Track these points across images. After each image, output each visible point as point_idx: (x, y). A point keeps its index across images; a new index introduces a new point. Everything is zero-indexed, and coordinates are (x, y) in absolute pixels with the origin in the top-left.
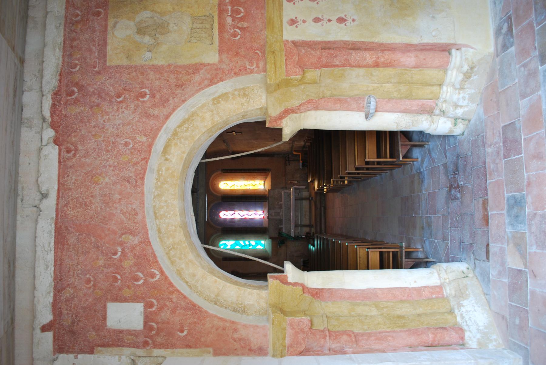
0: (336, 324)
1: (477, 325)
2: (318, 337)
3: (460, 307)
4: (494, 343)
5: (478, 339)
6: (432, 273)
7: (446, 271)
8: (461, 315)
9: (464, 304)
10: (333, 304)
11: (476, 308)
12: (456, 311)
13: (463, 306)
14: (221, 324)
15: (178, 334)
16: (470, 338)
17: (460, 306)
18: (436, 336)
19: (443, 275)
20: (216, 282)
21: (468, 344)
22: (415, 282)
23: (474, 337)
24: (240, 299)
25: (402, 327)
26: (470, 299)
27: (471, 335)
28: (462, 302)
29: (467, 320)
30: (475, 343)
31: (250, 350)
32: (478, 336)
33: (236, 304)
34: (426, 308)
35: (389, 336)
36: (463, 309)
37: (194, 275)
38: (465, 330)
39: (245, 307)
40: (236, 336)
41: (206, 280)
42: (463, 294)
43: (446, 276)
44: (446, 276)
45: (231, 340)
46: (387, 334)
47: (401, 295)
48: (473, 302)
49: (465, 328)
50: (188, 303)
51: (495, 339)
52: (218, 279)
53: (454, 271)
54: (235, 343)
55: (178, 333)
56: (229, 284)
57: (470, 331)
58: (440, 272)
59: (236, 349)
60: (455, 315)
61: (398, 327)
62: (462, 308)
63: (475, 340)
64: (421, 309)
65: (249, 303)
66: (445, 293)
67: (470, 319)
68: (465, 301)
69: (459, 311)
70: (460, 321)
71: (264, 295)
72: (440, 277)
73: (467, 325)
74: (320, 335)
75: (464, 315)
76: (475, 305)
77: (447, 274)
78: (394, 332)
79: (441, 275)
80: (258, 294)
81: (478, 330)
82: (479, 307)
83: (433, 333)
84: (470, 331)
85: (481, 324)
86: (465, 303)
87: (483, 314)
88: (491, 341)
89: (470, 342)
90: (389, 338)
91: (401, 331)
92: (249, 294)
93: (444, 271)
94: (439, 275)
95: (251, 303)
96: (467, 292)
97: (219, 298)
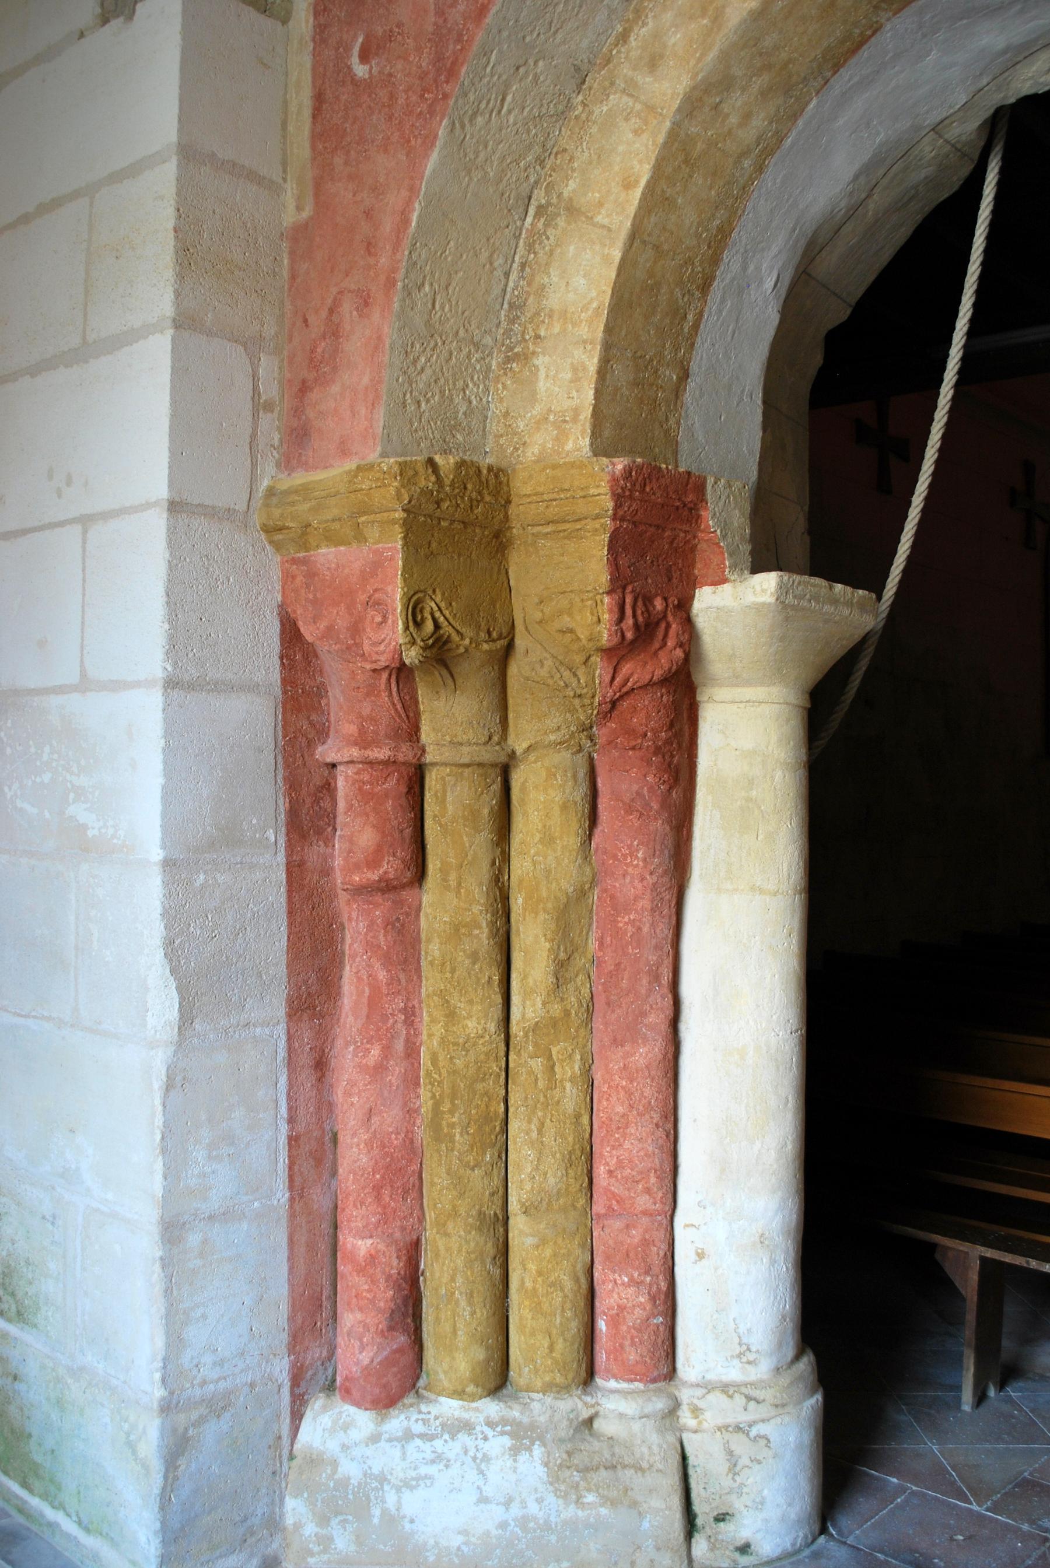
0: (450, 808)
1: (408, 1485)
2: (366, 709)
3: (512, 1435)
4: (310, 1529)
5: (335, 1464)
6: (744, 1354)
7: (738, 1429)
8: (467, 1427)
9: (524, 1456)
10: (564, 807)
11: (498, 1513)
12: (491, 1408)
13: (514, 1452)
14: (388, 226)
15: (355, 38)
16: (346, 1427)
17: (523, 1436)
18: (361, 1270)
19: (719, 1410)
20: (628, 185)
21: (325, 1409)
22: (701, 1255)
23: (345, 1447)
24: (557, 329)
25: (435, 1124)
26: (551, 1498)
27: (355, 1435)
28: (538, 1451)
29: (438, 1443)
30: (317, 1444)
31: (304, 389)
32: (350, 1469)
33: (537, 314)
34: (532, 1267)
35: (387, 1051)
36: (498, 1444)
37: (653, 63)
38: (383, 1418)
39: (525, 358)
40: (347, 308)
41: (637, 132)
42: (586, 1470)
43: (711, 1419)
44: (711, 1419)
45: (334, 290)
46: (399, 1046)
47: (620, 1164)
48: (533, 1508)
49: (397, 1422)
50: (459, 39)
51: (330, 1539)
52: (638, 193)
53: (733, 1469)
54: (324, 314)
55: (360, 40)
56: (617, 255)
57: (374, 1439)
58: (740, 1400)
59: (306, 321)
60: (473, 1398)
61: (437, 1105)
62: (507, 1441)
63: (332, 1446)
64: (530, 1241)
65: (542, 374)
66: (613, 1384)
67: (438, 1458)
68: (541, 1471)
69: (490, 1424)
70: (434, 1409)
71: (570, 446)
72: (708, 1387)
73: (408, 1436)
74: (372, 719)
75: (463, 1437)
76: (515, 1510)
77: (723, 1428)
78: (412, 1081)
79: (716, 1398)
80: (576, 412)
81: (382, 1479)
82: (503, 1525)
83: (372, 1258)
84: (374, 1439)
85: (411, 1503)
86: (532, 1466)
87: (465, 1532)
88: (323, 1520)
89: (326, 1420)
90: (375, 1052)
91: (411, 1112)
92: (575, 369)
93: (743, 1418)
94: (726, 1388)
95: (542, 385)
96: (590, 1498)
97: (561, 222)
